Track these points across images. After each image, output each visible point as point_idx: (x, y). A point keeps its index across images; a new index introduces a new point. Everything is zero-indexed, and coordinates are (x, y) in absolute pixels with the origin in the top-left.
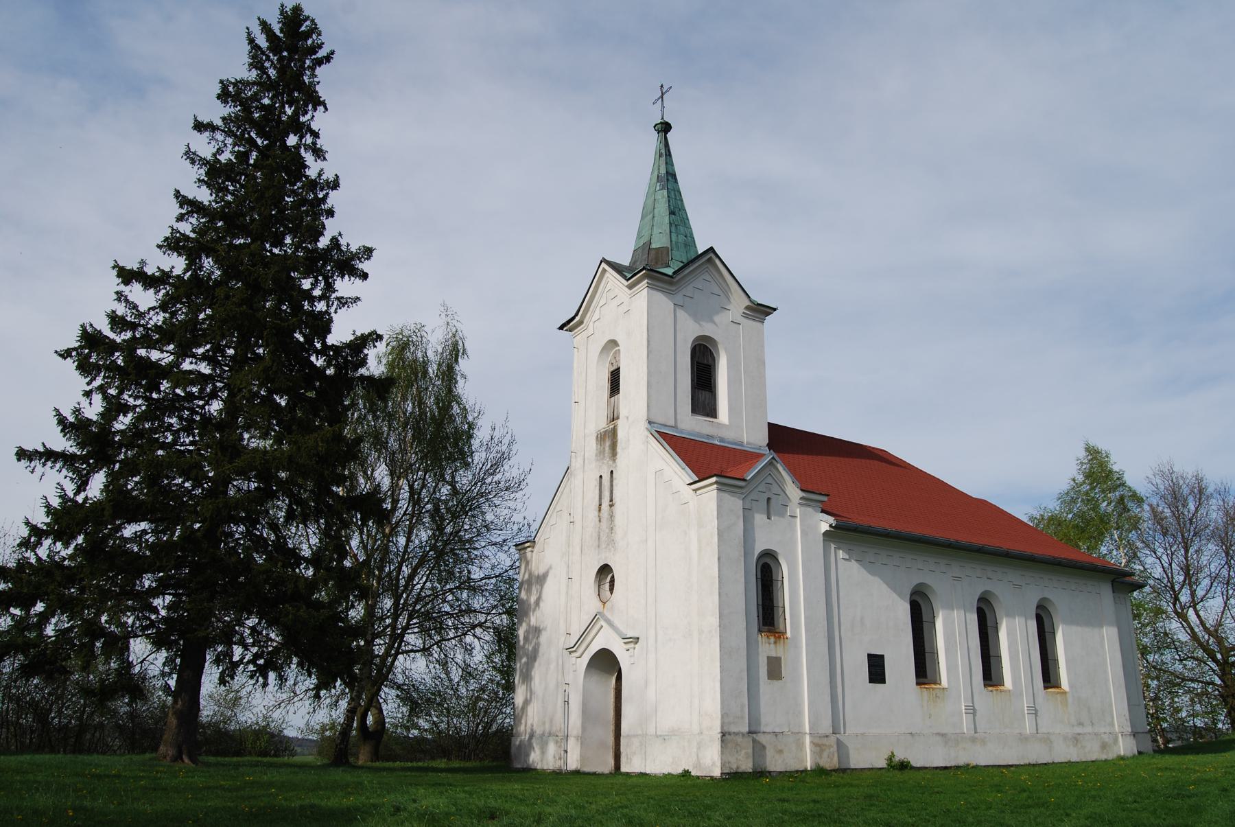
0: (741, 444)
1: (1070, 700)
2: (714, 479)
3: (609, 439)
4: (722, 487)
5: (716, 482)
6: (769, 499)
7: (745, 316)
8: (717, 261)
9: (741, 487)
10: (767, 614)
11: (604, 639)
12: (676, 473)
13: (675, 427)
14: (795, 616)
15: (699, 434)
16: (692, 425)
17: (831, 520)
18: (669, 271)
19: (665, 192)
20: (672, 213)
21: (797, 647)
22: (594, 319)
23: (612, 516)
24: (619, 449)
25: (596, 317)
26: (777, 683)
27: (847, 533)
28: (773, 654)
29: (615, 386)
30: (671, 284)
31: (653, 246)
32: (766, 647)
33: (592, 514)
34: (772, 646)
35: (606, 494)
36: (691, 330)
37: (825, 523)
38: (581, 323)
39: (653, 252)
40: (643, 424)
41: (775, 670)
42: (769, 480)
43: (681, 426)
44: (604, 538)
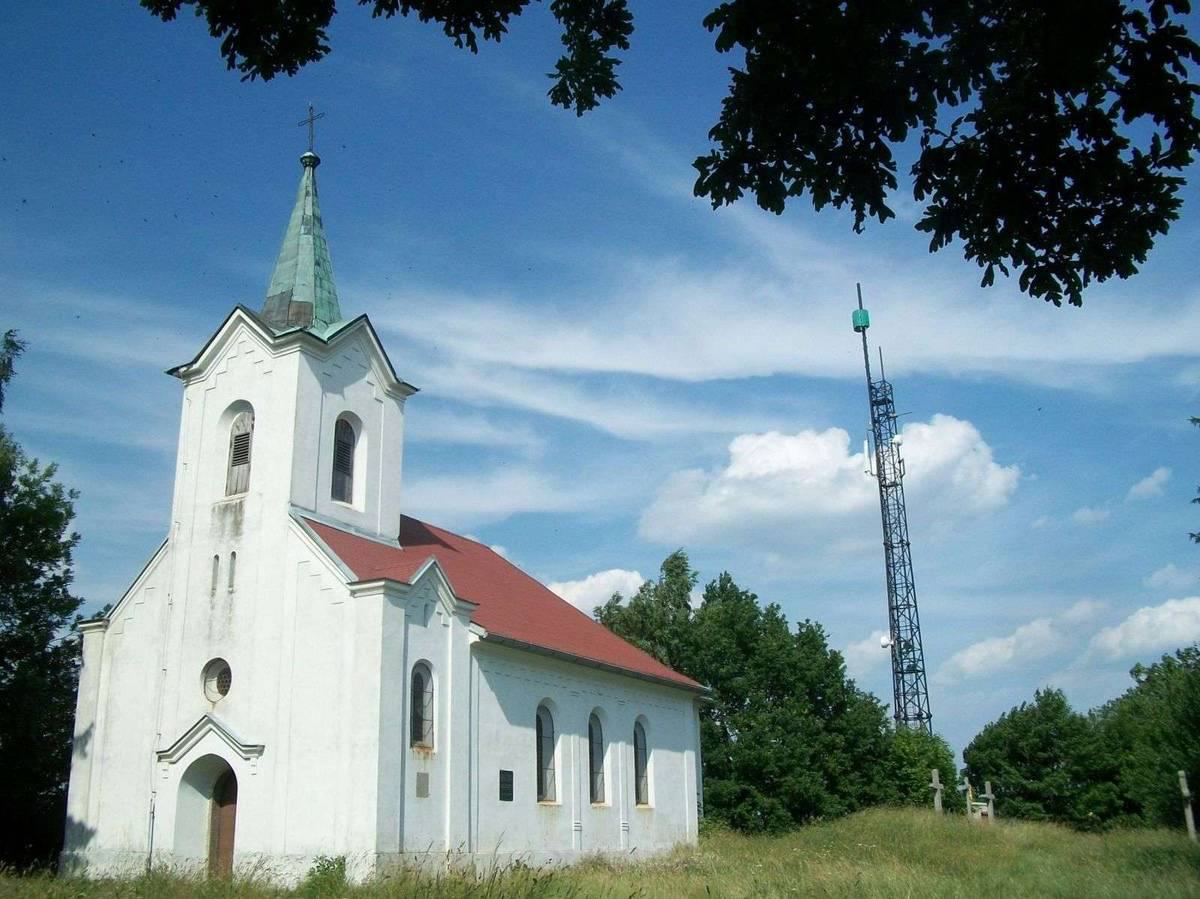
0: (374, 535)
1: (655, 815)
2: (382, 583)
3: (232, 514)
4: (388, 592)
5: (383, 586)
6: (426, 606)
7: (388, 394)
8: (368, 329)
9: (405, 592)
10: (418, 729)
11: (211, 745)
12: (331, 575)
13: (314, 512)
14: (442, 730)
15: (339, 523)
16: (332, 511)
17: (482, 632)
18: (325, 337)
19: (311, 238)
20: (317, 263)
21: (442, 762)
22: (217, 371)
23: (230, 606)
24: (245, 527)
25: (221, 367)
26: (425, 800)
27: (494, 650)
28: (422, 771)
29: (241, 450)
30: (322, 350)
31: (294, 298)
32: (415, 764)
33: (203, 599)
34: (422, 761)
35: (224, 578)
36: (336, 406)
37: (473, 635)
38: (198, 372)
39: (294, 305)
40: (284, 508)
41: (422, 789)
42: (429, 586)
43: (322, 510)
44: (217, 627)
